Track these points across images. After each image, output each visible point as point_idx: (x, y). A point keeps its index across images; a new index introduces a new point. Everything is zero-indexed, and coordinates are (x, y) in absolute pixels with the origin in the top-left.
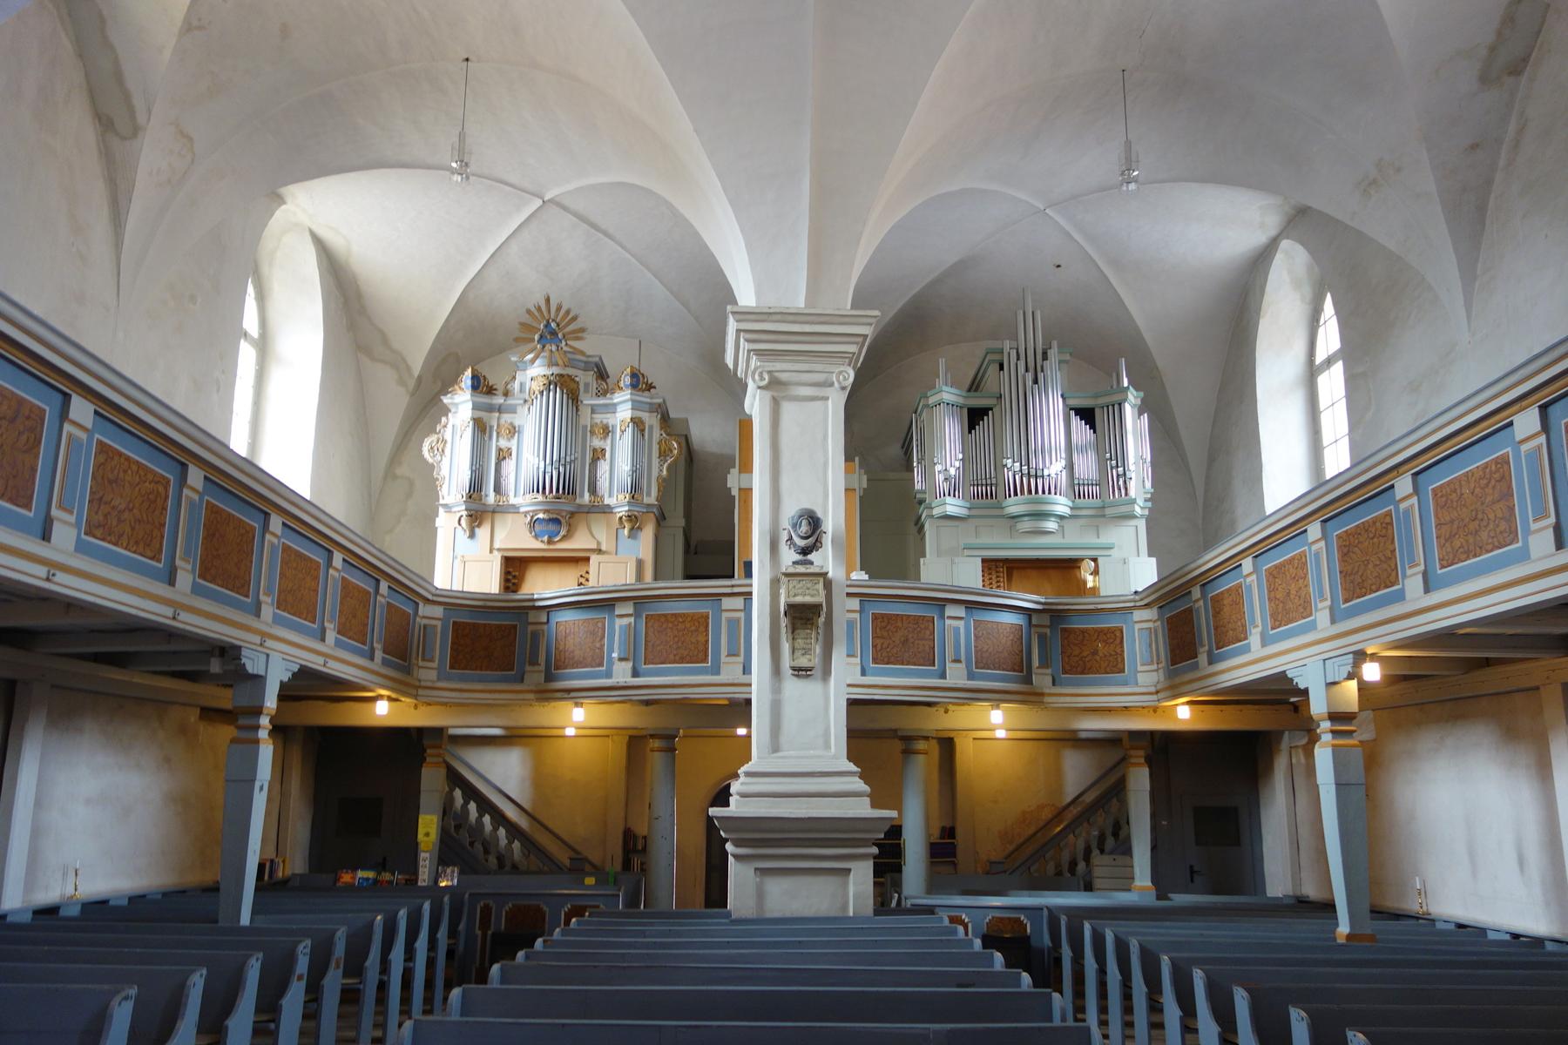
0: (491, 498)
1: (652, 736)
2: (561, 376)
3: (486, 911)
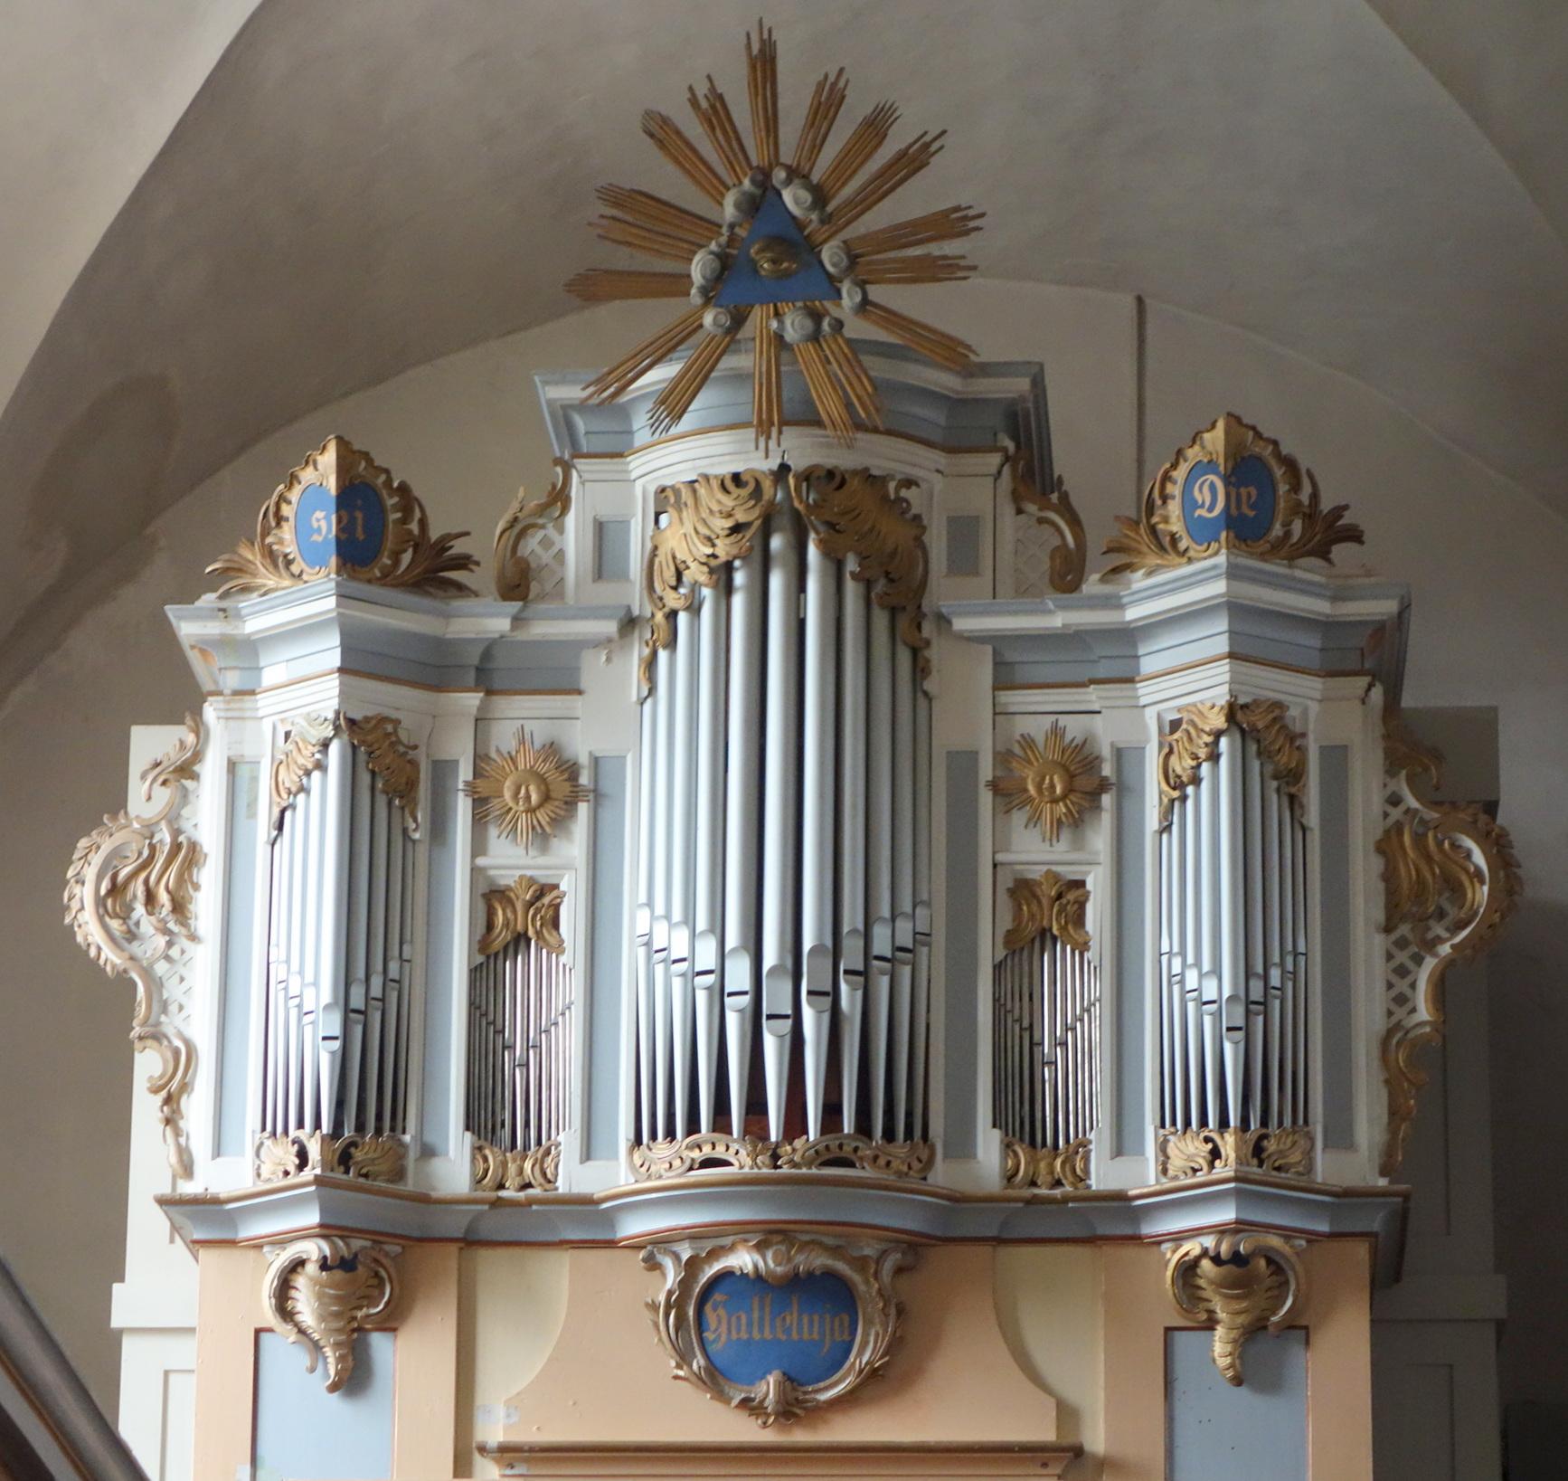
0: (454, 1166)
2: (831, 479)
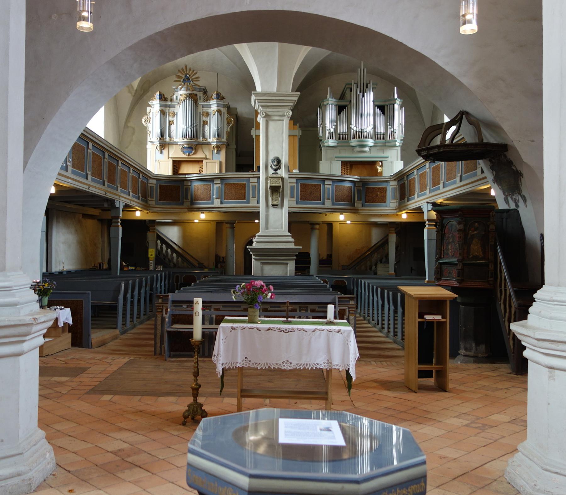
0: (167, 139)
1: (226, 223)
2: (191, 94)
3: (177, 277)
